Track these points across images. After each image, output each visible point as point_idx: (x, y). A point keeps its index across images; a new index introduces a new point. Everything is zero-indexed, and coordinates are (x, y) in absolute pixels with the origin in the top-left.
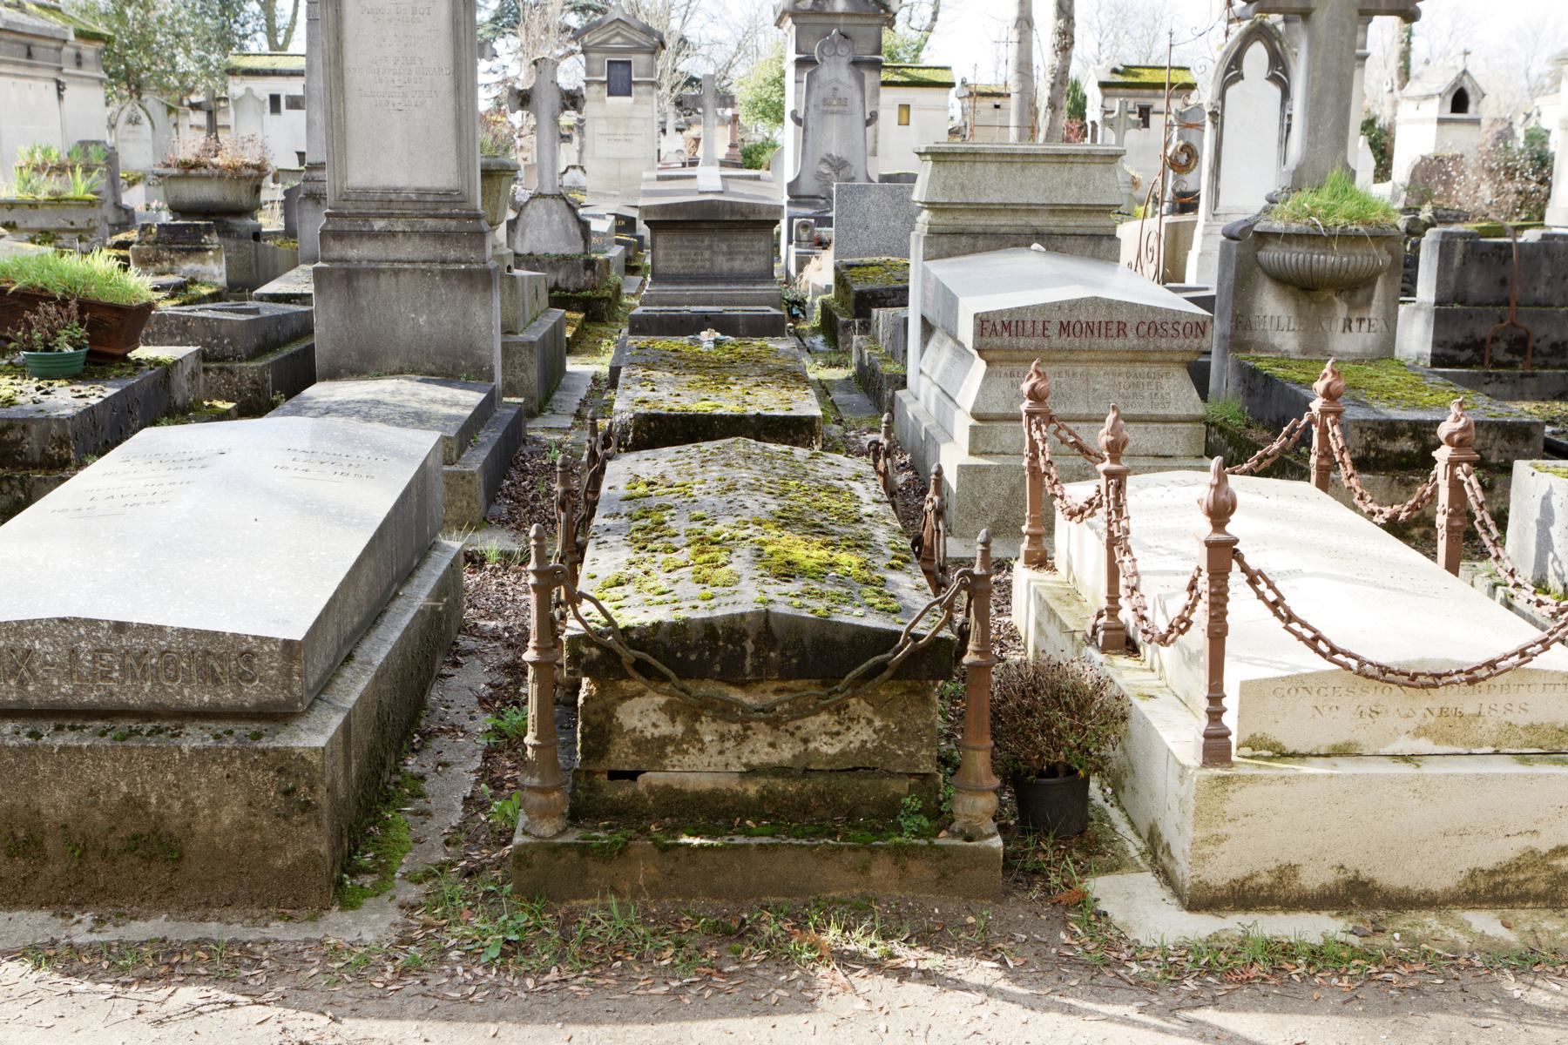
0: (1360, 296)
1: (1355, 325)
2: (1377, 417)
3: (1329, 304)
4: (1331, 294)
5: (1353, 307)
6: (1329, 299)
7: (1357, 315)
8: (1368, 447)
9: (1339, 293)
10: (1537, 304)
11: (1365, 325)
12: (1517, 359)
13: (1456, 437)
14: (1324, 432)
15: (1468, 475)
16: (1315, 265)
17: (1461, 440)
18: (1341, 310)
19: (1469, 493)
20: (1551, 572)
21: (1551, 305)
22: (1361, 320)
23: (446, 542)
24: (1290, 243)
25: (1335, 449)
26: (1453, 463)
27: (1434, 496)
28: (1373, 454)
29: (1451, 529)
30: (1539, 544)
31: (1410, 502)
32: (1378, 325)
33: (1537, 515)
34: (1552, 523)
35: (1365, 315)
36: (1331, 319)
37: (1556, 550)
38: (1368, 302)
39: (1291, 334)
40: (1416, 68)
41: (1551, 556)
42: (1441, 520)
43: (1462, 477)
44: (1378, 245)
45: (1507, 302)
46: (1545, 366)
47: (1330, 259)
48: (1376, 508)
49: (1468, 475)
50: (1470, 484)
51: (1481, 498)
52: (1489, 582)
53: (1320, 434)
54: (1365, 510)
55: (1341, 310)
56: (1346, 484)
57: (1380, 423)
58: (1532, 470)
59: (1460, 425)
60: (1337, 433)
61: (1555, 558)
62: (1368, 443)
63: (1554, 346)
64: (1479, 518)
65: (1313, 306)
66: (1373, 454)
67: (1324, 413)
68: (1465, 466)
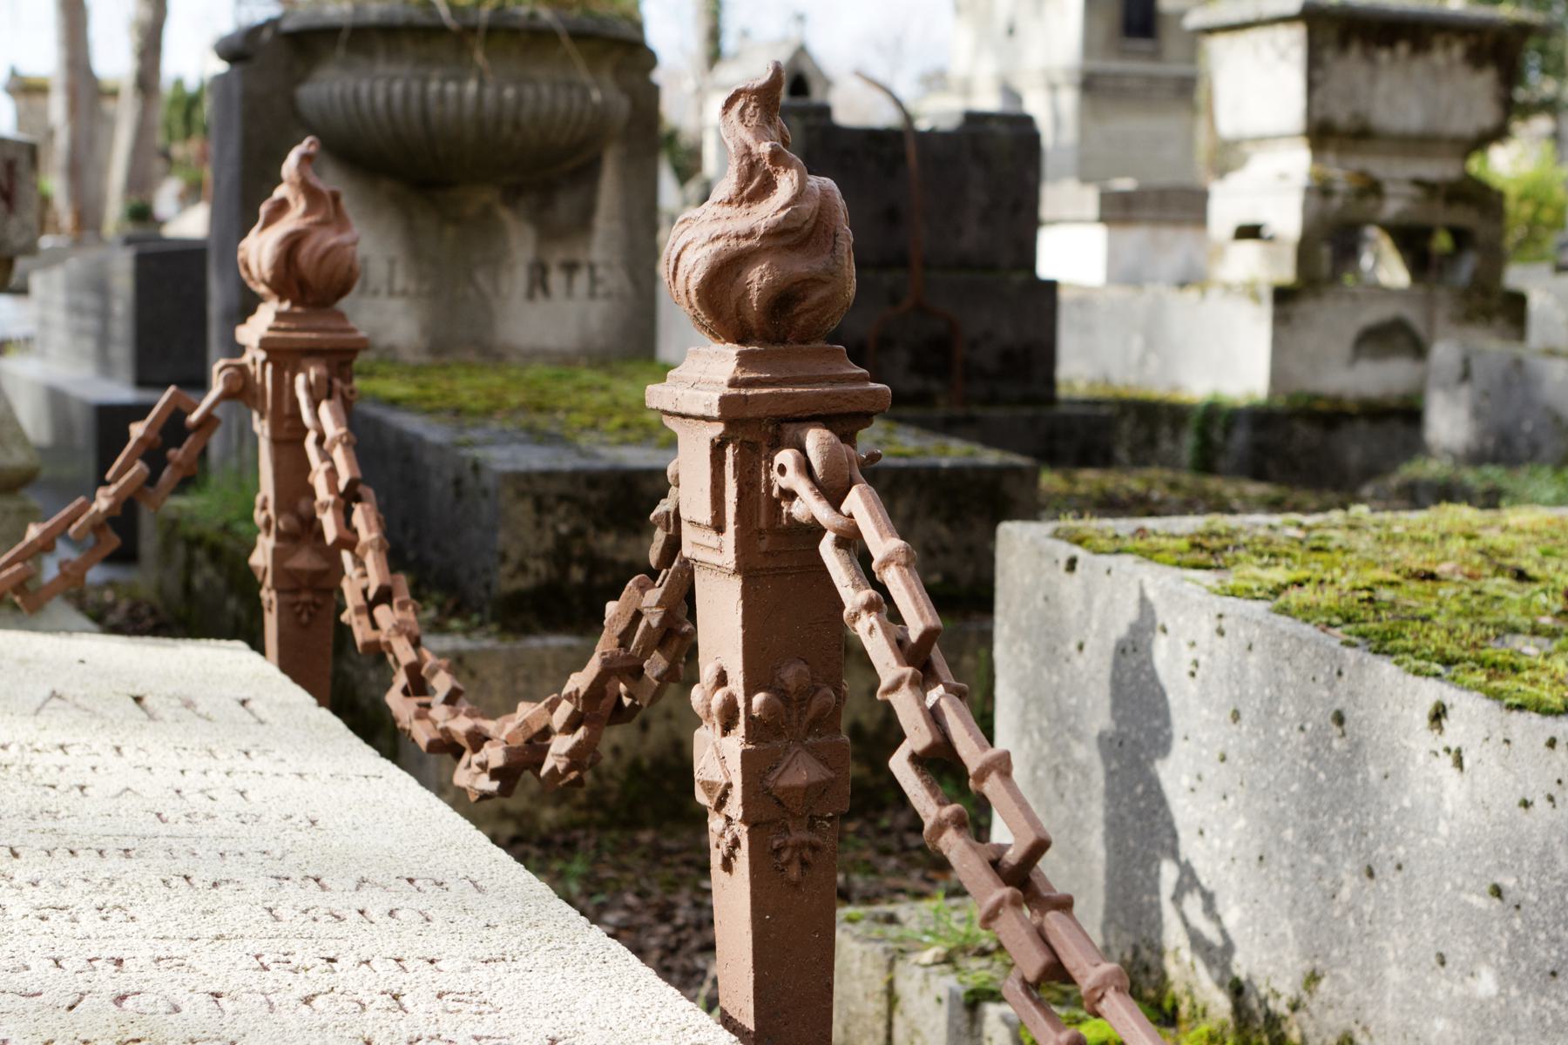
0: (565, 206)
1: (556, 279)
2: (582, 463)
3: (486, 227)
4: (487, 195)
5: (548, 234)
6: (487, 212)
7: (556, 256)
8: (561, 555)
9: (512, 195)
10: (964, 264)
11: (581, 281)
12: (935, 386)
13: (757, 277)
14: (290, 437)
15: (834, 494)
16: (435, 110)
17: (782, 301)
18: (521, 243)
19: (852, 596)
20: (1174, 936)
21: (991, 267)
22: (570, 268)
23: (956, 806)
24: (370, 53)
25: (323, 493)
26: (750, 431)
27: (677, 632)
28: (577, 574)
29: (767, 808)
30: (1115, 827)
31: (579, 681)
32: (614, 279)
33: (1099, 717)
34: (1163, 746)
35: (580, 255)
36: (497, 263)
37: (1190, 847)
38: (584, 222)
39: (397, 304)
40: (729, 43)
41: (1169, 873)
42: (718, 758)
43: (808, 505)
44: (593, 62)
45: (902, 261)
46: (992, 400)
47: (466, 91)
48: (461, 725)
49: (834, 494)
50: (850, 541)
51: (917, 618)
52: (947, 983)
53: (276, 442)
54: (422, 734)
55: (521, 243)
56: (361, 633)
57: (593, 479)
58: (1065, 550)
59: (768, 212)
60: (332, 429)
61: (1188, 880)
62: (563, 543)
63: (1007, 356)
64: (918, 737)
65: (450, 232)
66: (577, 574)
67: (282, 355)
68: (815, 440)
